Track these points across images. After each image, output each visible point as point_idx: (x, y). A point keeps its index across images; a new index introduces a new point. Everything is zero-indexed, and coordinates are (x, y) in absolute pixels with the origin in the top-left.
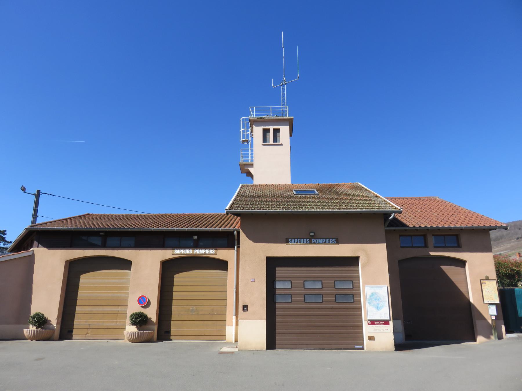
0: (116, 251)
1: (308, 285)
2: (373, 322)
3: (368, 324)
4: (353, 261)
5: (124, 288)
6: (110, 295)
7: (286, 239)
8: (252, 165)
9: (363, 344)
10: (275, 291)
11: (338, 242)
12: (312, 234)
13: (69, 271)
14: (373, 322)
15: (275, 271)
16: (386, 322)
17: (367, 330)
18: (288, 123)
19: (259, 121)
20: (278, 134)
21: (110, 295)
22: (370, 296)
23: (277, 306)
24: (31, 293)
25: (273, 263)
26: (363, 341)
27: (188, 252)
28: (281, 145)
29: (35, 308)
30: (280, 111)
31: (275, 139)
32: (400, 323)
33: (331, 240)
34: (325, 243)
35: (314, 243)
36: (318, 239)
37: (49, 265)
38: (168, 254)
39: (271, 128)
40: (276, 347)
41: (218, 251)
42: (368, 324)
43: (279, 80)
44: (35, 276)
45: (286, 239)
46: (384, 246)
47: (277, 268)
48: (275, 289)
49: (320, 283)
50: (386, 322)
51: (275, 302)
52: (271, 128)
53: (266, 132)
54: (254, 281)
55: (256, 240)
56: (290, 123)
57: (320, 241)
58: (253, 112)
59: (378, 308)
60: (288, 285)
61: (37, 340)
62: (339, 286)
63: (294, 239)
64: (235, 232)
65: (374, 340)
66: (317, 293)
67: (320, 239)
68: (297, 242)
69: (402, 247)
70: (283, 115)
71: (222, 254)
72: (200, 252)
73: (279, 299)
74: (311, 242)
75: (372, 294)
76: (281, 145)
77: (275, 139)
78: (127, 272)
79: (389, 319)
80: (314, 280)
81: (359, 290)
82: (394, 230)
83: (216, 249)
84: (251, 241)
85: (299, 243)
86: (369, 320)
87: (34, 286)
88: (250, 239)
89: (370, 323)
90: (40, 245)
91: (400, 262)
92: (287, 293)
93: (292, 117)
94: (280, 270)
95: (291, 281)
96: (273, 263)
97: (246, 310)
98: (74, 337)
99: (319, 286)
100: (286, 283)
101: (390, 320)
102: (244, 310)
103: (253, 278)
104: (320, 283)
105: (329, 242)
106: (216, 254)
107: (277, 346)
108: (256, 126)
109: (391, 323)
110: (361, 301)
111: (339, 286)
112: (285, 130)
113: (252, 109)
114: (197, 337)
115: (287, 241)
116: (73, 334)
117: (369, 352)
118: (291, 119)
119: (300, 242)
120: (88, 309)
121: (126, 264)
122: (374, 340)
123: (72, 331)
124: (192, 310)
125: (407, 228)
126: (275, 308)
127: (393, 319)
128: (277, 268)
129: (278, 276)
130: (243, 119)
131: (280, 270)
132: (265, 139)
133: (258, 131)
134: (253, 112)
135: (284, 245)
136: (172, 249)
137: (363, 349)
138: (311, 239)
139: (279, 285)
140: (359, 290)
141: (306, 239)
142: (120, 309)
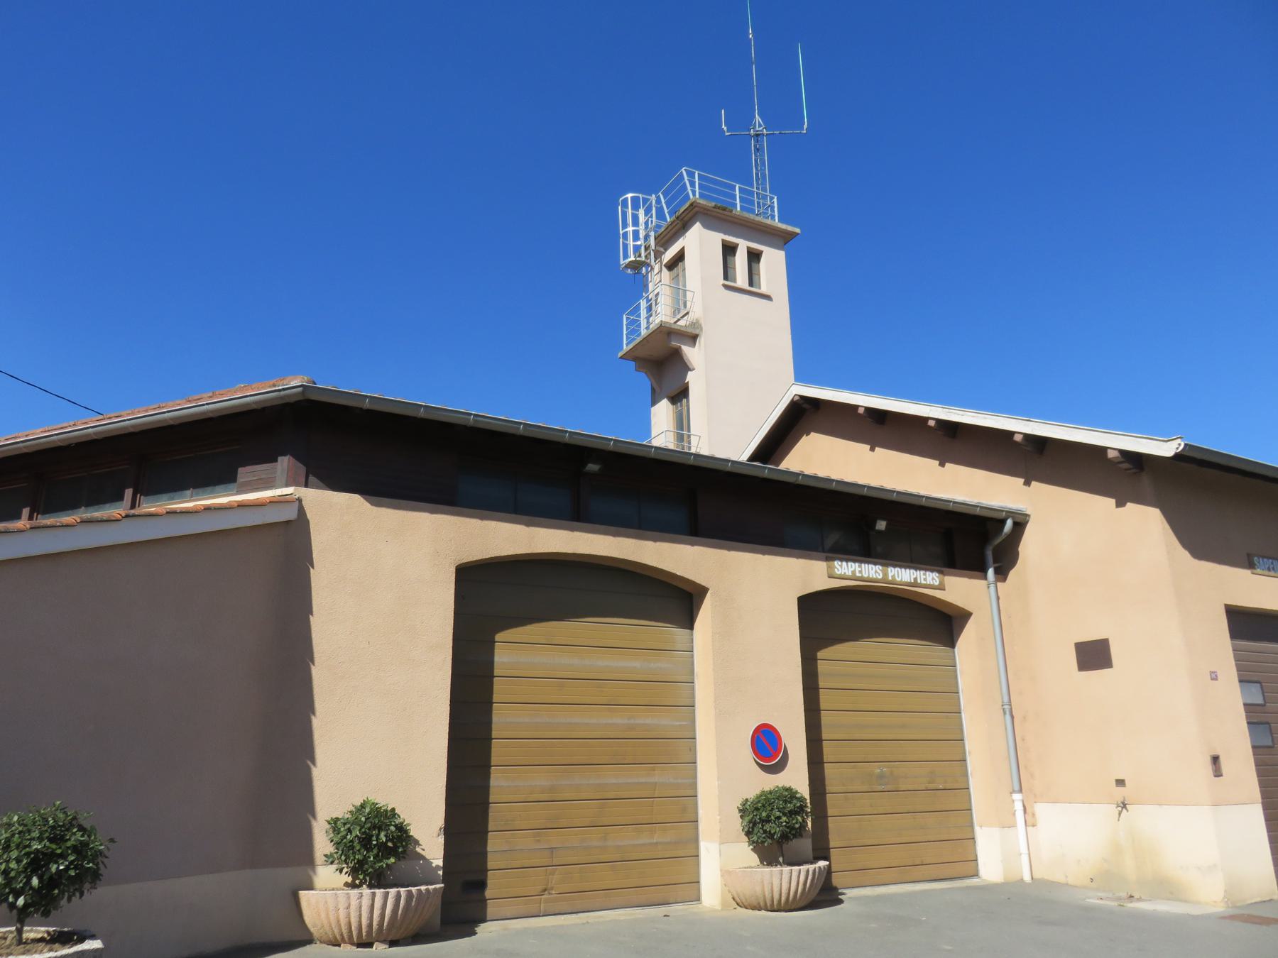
0: (650, 544)
5: (675, 694)
6: (619, 719)
8: (693, 339)
13: (921, 604)
21: (619, 719)
24: (310, 708)
27: (870, 572)
29: (337, 788)
31: (752, 276)
37: (382, 578)
38: (818, 574)
39: (743, 245)
43: (741, 120)
44: (316, 622)
61: (393, 943)
64: (1009, 523)
70: (765, 215)
71: (957, 589)
72: (902, 576)
76: (768, 297)
77: (752, 276)
78: (679, 633)
87: (319, 674)
90: (311, 478)
98: (492, 909)
114: (905, 872)
115: (1251, 565)
116: (488, 893)
120: (539, 780)
121: (681, 601)
123: (482, 885)
124: (881, 776)
136: (827, 559)
142: (659, 777)
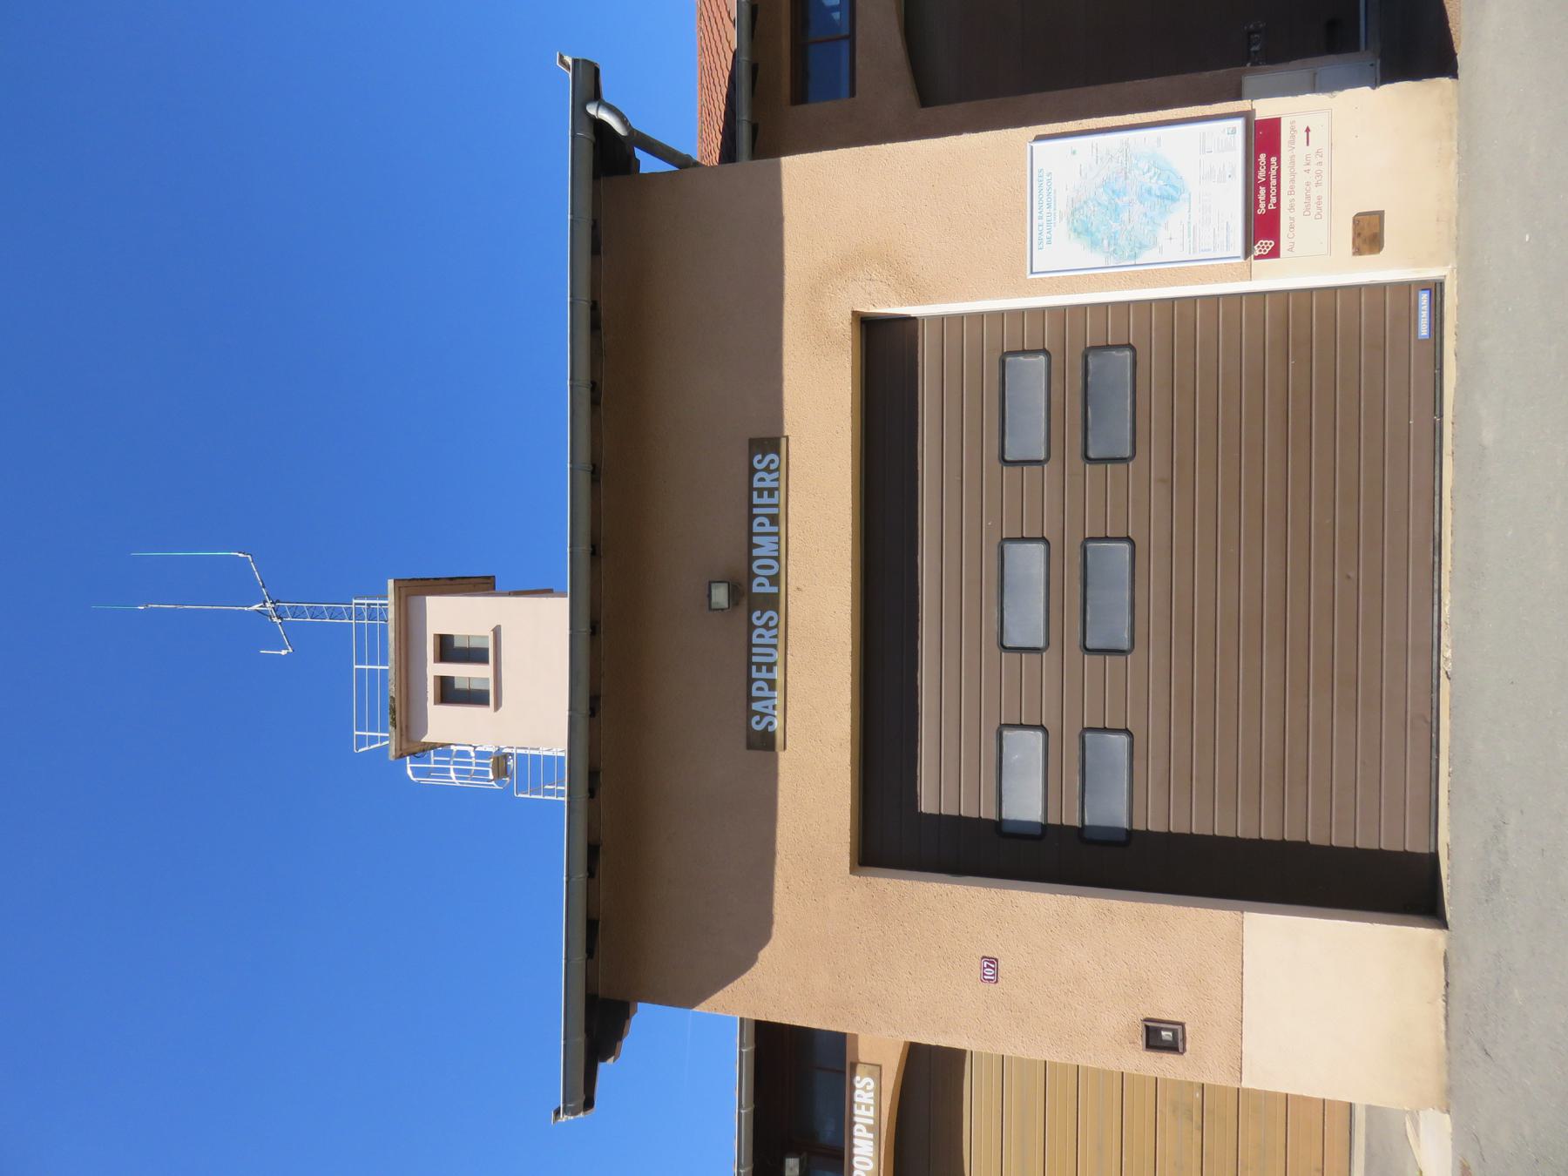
1: (1026, 624)
2: (1263, 227)
3: (1275, 253)
4: (885, 349)
7: (750, 746)
9: (1406, 290)
10: (1061, 828)
11: (770, 443)
12: (720, 595)
14: (1263, 227)
15: (939, 818)
16: (1264, 140)
17: (1314, 259)
18: (414, 600)
19: (405, 718)
20: (457, 644)
22: (1094, 244)
23: (1154, 823)
25: (896, 832)
26: (1381, 288)
28: (497, 632)
30: (359, 627)
31: (475, 655)
32: (1250, 81)
33: (762, 480)
34: (774, 520)
35: (775, 580)
36: (751, 559)
40: (1422, 848)
41: (862, 1057)
42: (1275, 253)
45: (750, 746)
46: (786, 161)
47: (927, 805)
48: (1045, 827)
49: (1012, 550)
50: (1264, 140)
51: (1130, 833)
52: (435, 669)
53: (448, 693)
54: (993, 961)
55: (759, 929)
56: (415, 588)
57: (764, 546)
58: (373, 740)
59: (1170, 196)
60: (1025, 749)
62: (1029, 438)
63: (750, 699)
65: (1380, 215)
66: (1073, 586)
67: (751, 546)
68: (772, 684)
69: (853, 93)
73: (1110, 809)
74: (772, 602)
75: (1083, 231)
76: (497, 632)
77: (475, 655)
79: (1239, 124)
80: (997, 593)
81: (1061, 312)
82: (755, 130)
83: (854, 1066)
84: (764, 954)
85: (777, 674)
86: (1248, 252)
88: (748, 961)
89: (1265, 245)
91: (925, 98)
92: (1070, 762)
93: (391, 583)
94: (936, 793)
95: (1003, 726)
96: (896, 832)
97: (1178, 1028)
99: (1029, 562)
100: (1012, 756)
101: (1247, 116)
102: (1173, 1047)
103: (977, 964)
104: (1012, 550)
105: (771, 492)
106: (877, 1071)
107: (1414, 844)
108: (425, 732)
109: (1265, 108)
110: (1127, 305)
111: (1029, 438)
112: (447, 615)
113: (361, 741)
115: (765, 743)
117: (1467, 252)
118: (398, 588)
119: (770, 667)
122: (1380, 215)
125: (744, 58)
126: (1169, 837)
127: (1238, 96)
128: (927, 805)
129: (974, 805)
130: (417, 772)
131: (936, 793)
132: (476, 697)
133: (442, 723)
134: (373, 740)
135: (787, 761)
137: (1436, 289)
138: (753, 597)
139: (1025, 803)
140: (1061, 314)
141: (751, 627)
